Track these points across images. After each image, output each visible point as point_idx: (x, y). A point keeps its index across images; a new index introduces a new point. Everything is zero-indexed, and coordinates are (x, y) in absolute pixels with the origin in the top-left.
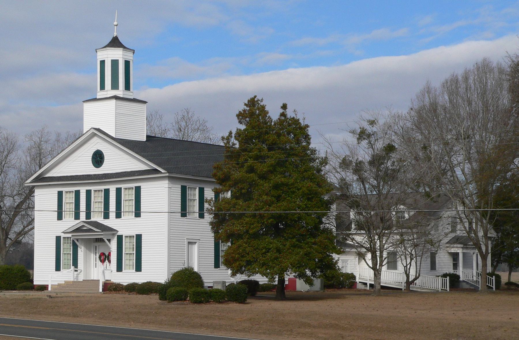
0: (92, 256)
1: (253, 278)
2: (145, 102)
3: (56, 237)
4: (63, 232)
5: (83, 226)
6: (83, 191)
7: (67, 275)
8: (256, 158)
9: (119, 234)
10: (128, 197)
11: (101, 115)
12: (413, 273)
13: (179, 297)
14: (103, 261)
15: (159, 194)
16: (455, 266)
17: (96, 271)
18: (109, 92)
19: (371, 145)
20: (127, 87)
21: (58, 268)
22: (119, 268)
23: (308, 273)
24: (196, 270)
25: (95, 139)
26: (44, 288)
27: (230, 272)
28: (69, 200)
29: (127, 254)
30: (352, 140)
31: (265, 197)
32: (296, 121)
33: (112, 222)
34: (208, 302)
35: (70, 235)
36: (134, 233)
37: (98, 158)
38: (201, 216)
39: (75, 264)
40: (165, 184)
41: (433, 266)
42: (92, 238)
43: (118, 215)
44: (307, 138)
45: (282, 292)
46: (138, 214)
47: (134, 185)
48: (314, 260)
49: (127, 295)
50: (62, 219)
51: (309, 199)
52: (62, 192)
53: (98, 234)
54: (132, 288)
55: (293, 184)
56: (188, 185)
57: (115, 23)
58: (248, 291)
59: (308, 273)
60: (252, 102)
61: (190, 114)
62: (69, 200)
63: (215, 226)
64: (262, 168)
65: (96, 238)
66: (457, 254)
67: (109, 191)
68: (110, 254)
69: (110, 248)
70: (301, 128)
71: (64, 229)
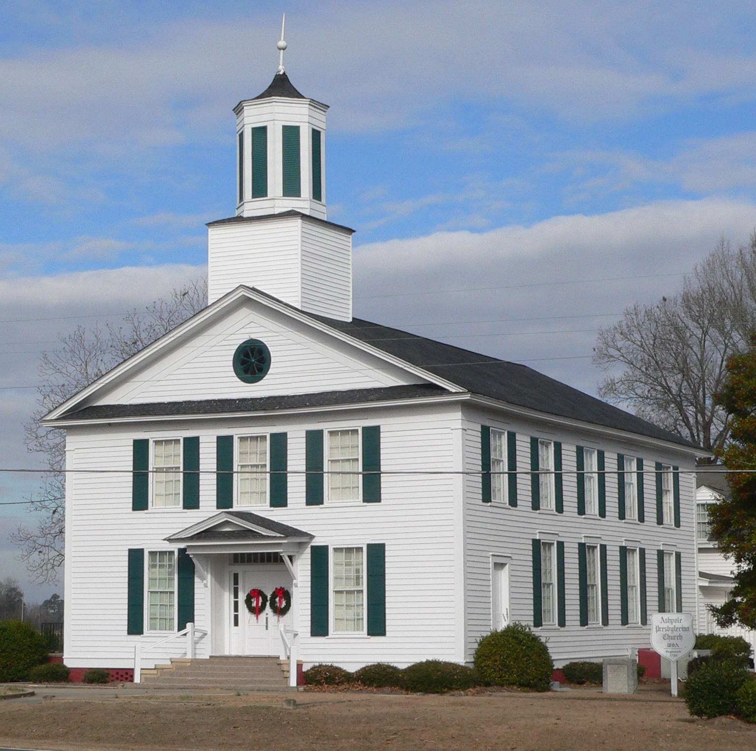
2: (350, 231)
3: (130, 551)
4: (169, 540)
5: (226, 523)
9: (316, 542)
10: (342, 452)
17: (227, 631)
18: (278, 203)
20: (317, 194)
21: (135, 626)
22: (319, 627)
28: (165, 458)
29: (341, 592)
33: (296, 513)
36: (363, 540)
37: (252, 360)
39: (186, 614)
40: (454, 419)
43: (314, 496)
46: (372, 492)
50: (147, 508)
52: (230, 439)
54: (378, 677)
57: (282, 43)
62: (165, 458)
65: (235, 554)
67: (379, 432)
71: (169, 533)
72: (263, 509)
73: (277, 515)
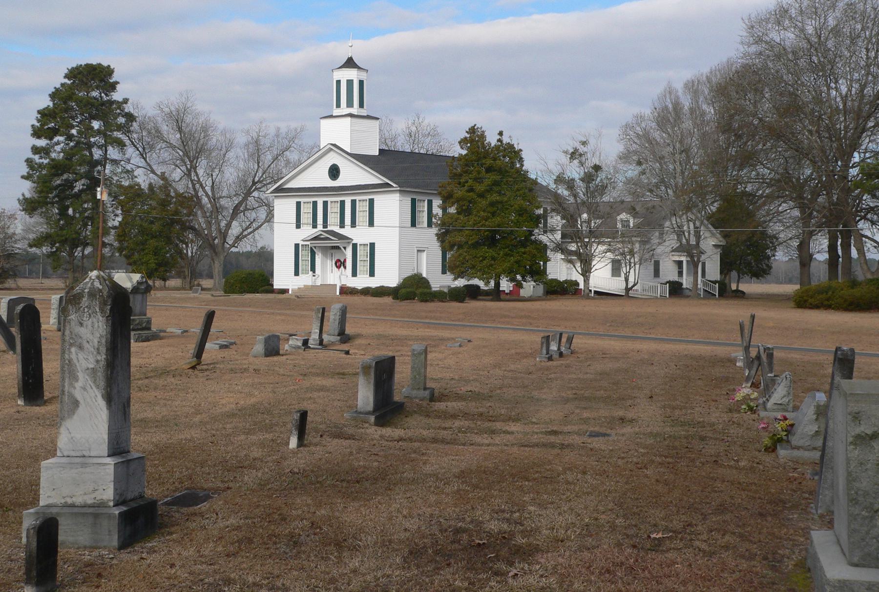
0: (329, 262)
1: (471, 282)
2: (378, 119)
6: (320, 202)
7: (305, 280)
8: (475, 179)
9: (354, 242)
11: (338, 132)
12: (631, 280)
13: (409, 297)
14: (338, 267)
15: (391, 207)
16: (680, 274)
17: (331, 276)
19: (582, 164)
20: (361, 105)
21: (297, 273)
22: (354, 274)
23: (519, 277)
24: (424, 275)
25: (332, 154)
26: (285, 291)
27: (452, 277)
28: (306, 210)
30: (565, 159)
31: (482, 213)
32: (511, 146)
33: (347, 231)
34: (433, 301)
35: (308, 243)
36: (368, 241)
37: (334, 172)
38: (430, 224)
39: (313, 269)
40: (396, 197)
41: (657, 273)
42: (329, 245)
43: (353, 224)
44: (521, 160)
45: (496, 294)
46: (371, 223)
47: (368, 197)
48: (525, 267)
49: (363, 297)
51: (520, 215)
53: (335, 242)
54: (366, 292)
55: (506, 202)
56: (417, 197)
58: (473, 293)
59: (519, 277)
60: (472, 130)
61: (421, 120)
62: (306, 210)
63: (441, 237)
64: (480, 188)
66: (682, 261)
68: (345, 260)
69: (345, 255)
70: (515, 152)
72: (337, 229)
73: (342, 231)
